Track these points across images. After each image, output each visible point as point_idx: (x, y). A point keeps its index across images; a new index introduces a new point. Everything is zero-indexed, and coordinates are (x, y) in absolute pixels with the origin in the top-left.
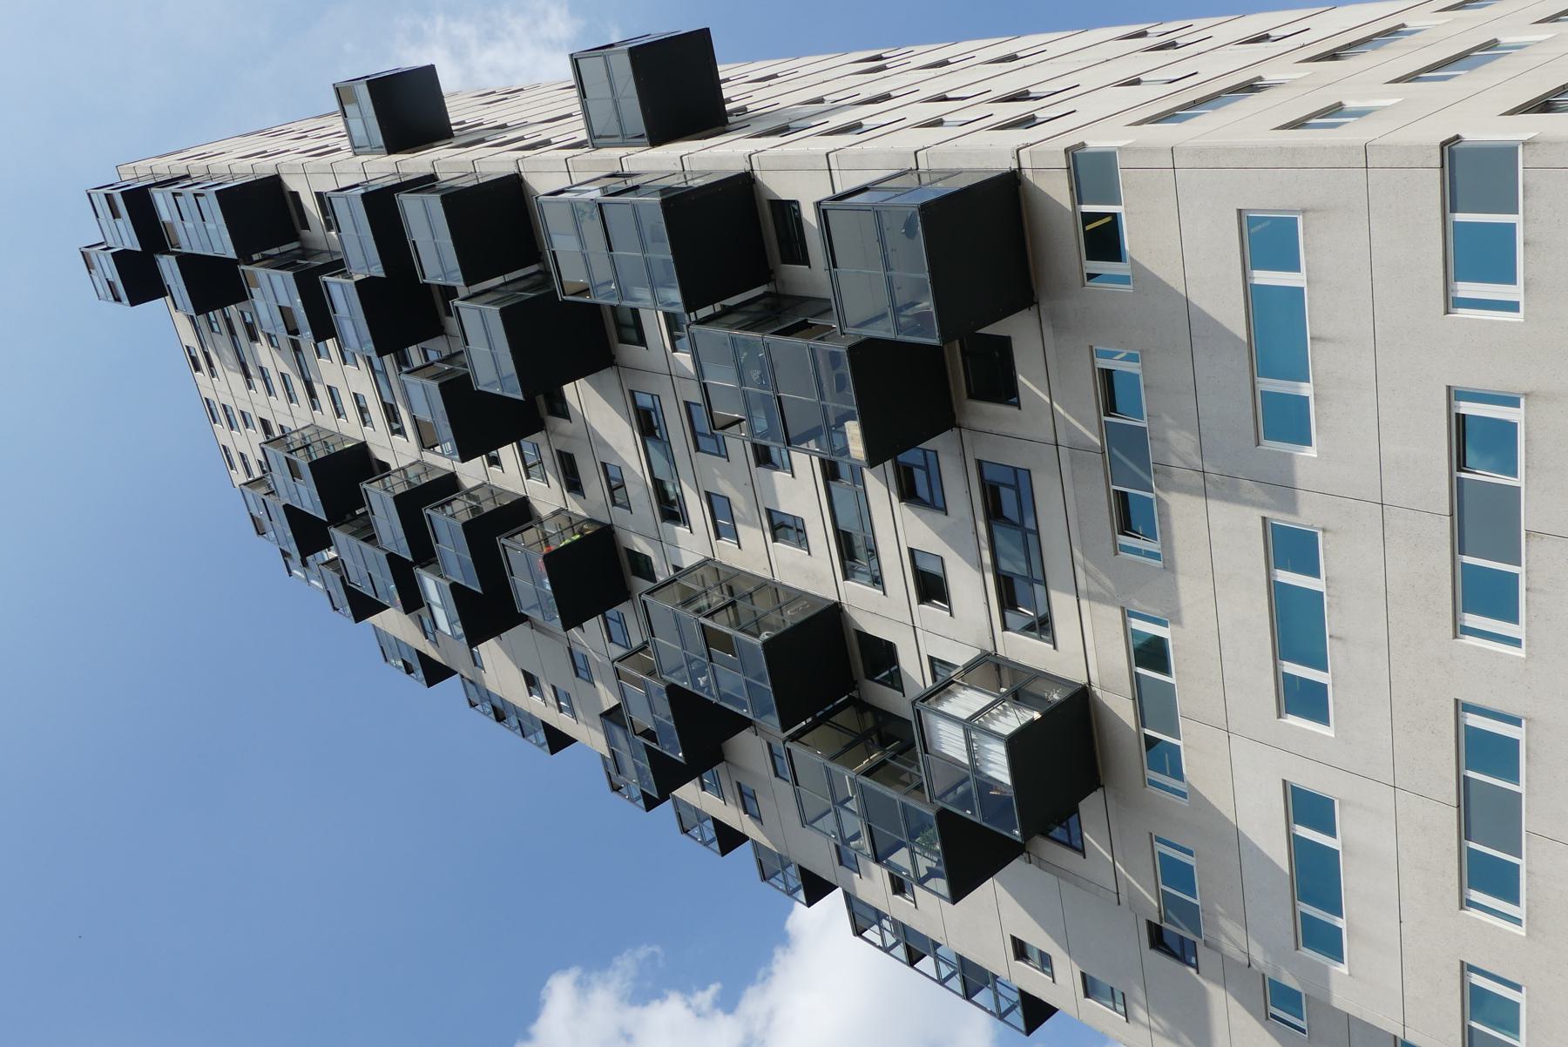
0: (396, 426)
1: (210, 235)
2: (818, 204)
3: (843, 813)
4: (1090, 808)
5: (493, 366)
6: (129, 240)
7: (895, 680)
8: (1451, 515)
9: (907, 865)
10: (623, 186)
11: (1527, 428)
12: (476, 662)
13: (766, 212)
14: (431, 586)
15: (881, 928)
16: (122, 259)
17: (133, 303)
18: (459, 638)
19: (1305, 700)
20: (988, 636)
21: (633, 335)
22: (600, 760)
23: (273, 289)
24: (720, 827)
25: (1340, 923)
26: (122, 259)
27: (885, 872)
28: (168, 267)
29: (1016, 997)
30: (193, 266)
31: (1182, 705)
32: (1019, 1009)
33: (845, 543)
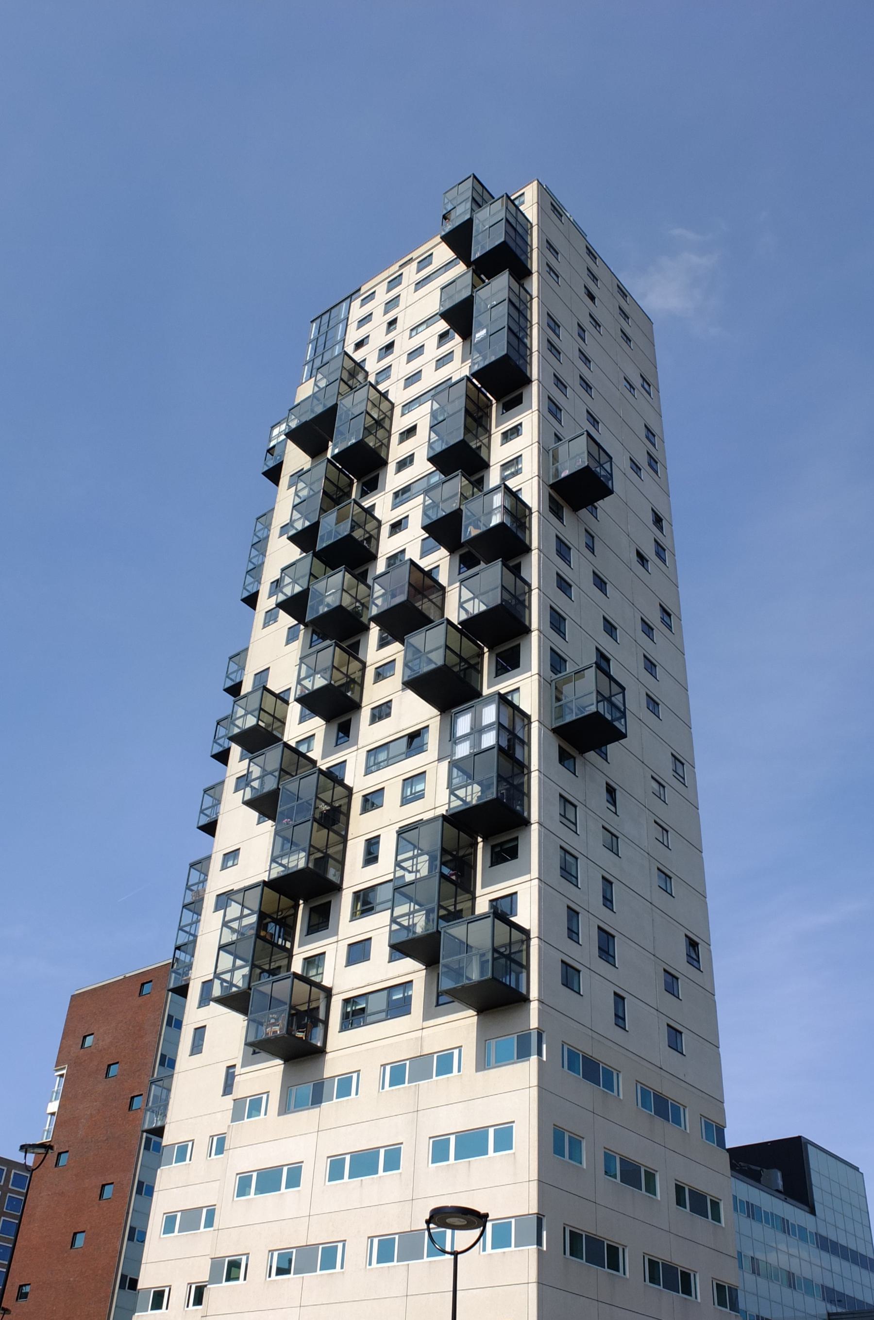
7: (364, 494)
9: (286, 583)
10: (517, 305)
12: (270, 617)
18: (312, 411)
19: (336, 1171)
22: (245, 647)
25: (252, 1195)
27: (279, 577)
29: (238, 680)
32: (233, 683)
33: (406, 490)
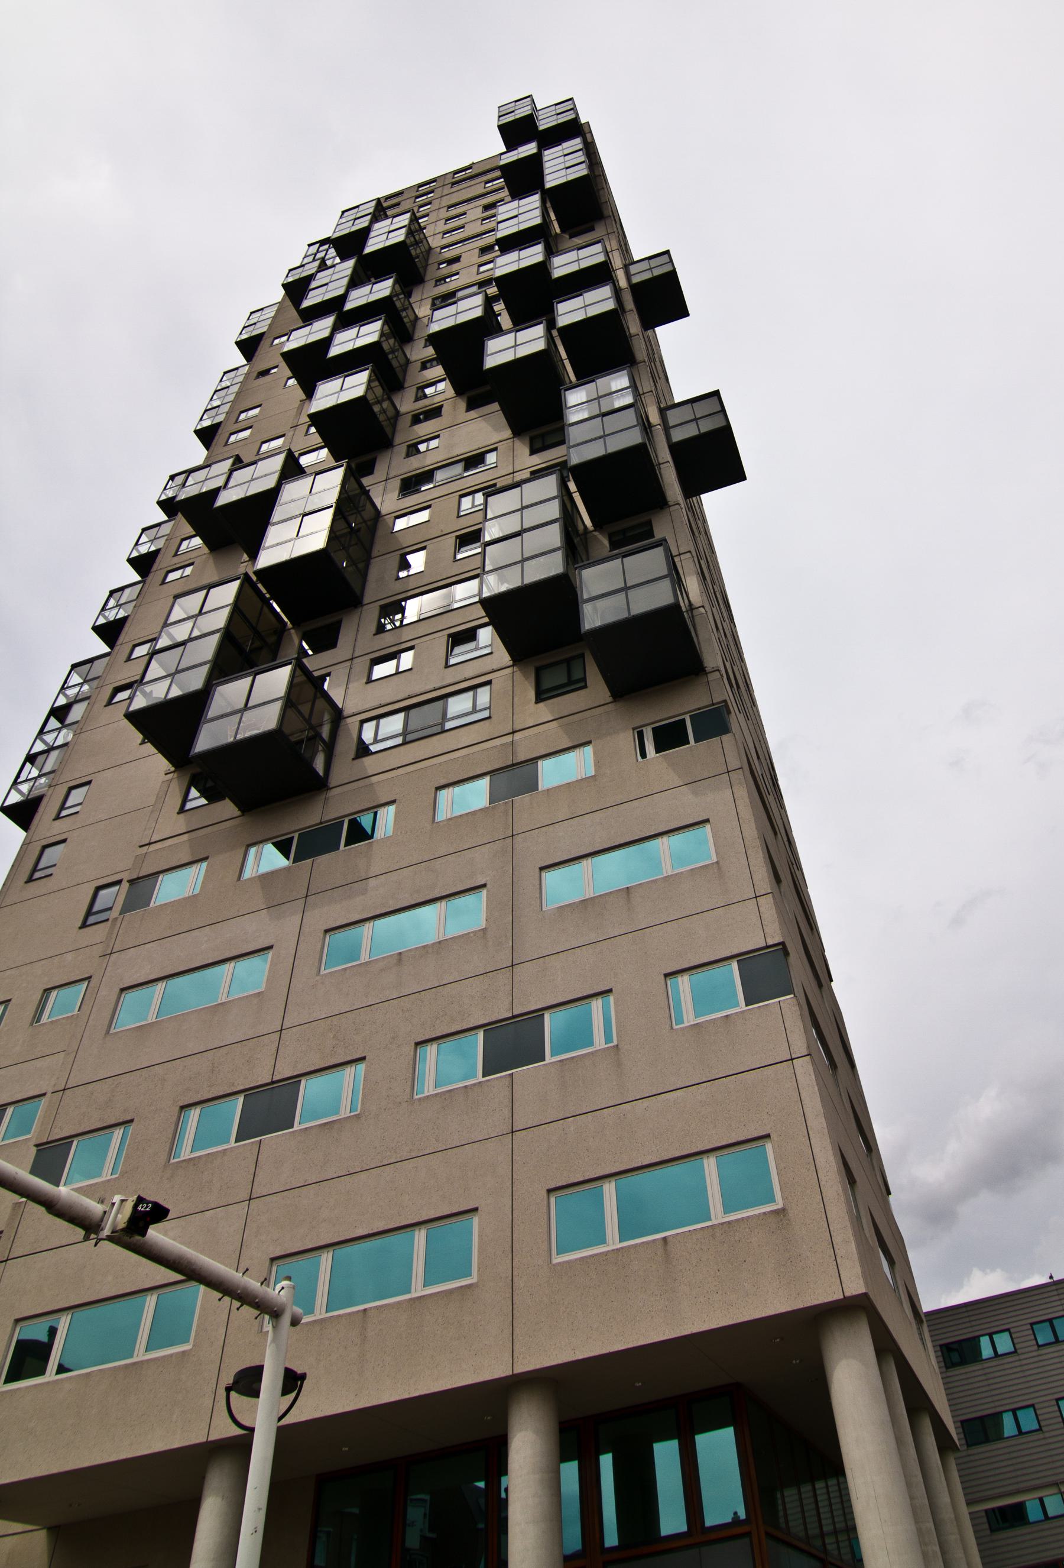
0: (437, 302)
1: (560, 166)
2: (665, 540)
3: (168, 681)
4: (227, 808)
5: (501, 351)
6: (544, 123)
8: (514, 1017)
11: (592, 1053)
13: (642, 518)
14: (321, 328)
15: (82, 684)
16: (529, 121)
17: (499, 127)
20: (355, 711)
21: (538, 445)
23: (528, 211)
24: (68, 1370)
26: (529, 121)
28: (529, 149)
30: (535, 164)
31: (324, 859)
